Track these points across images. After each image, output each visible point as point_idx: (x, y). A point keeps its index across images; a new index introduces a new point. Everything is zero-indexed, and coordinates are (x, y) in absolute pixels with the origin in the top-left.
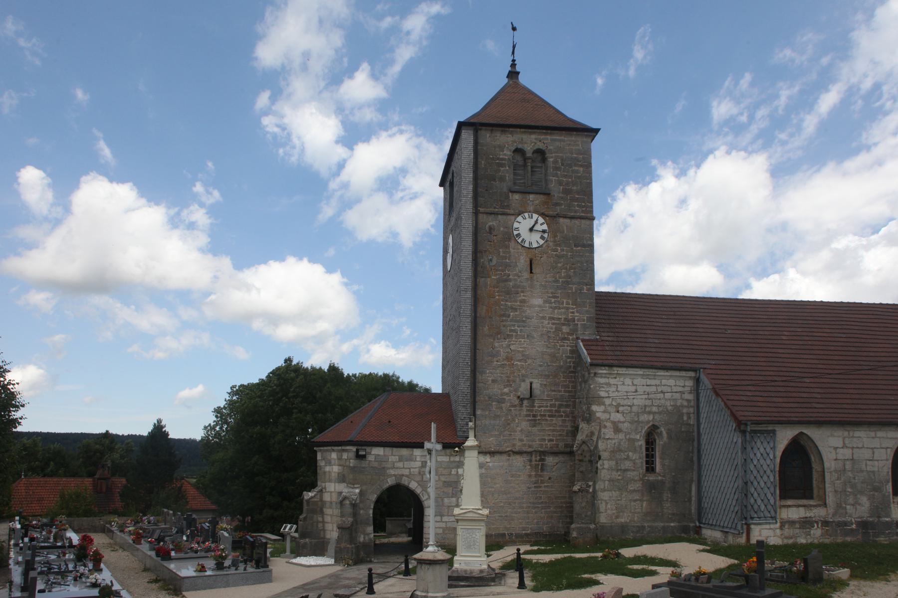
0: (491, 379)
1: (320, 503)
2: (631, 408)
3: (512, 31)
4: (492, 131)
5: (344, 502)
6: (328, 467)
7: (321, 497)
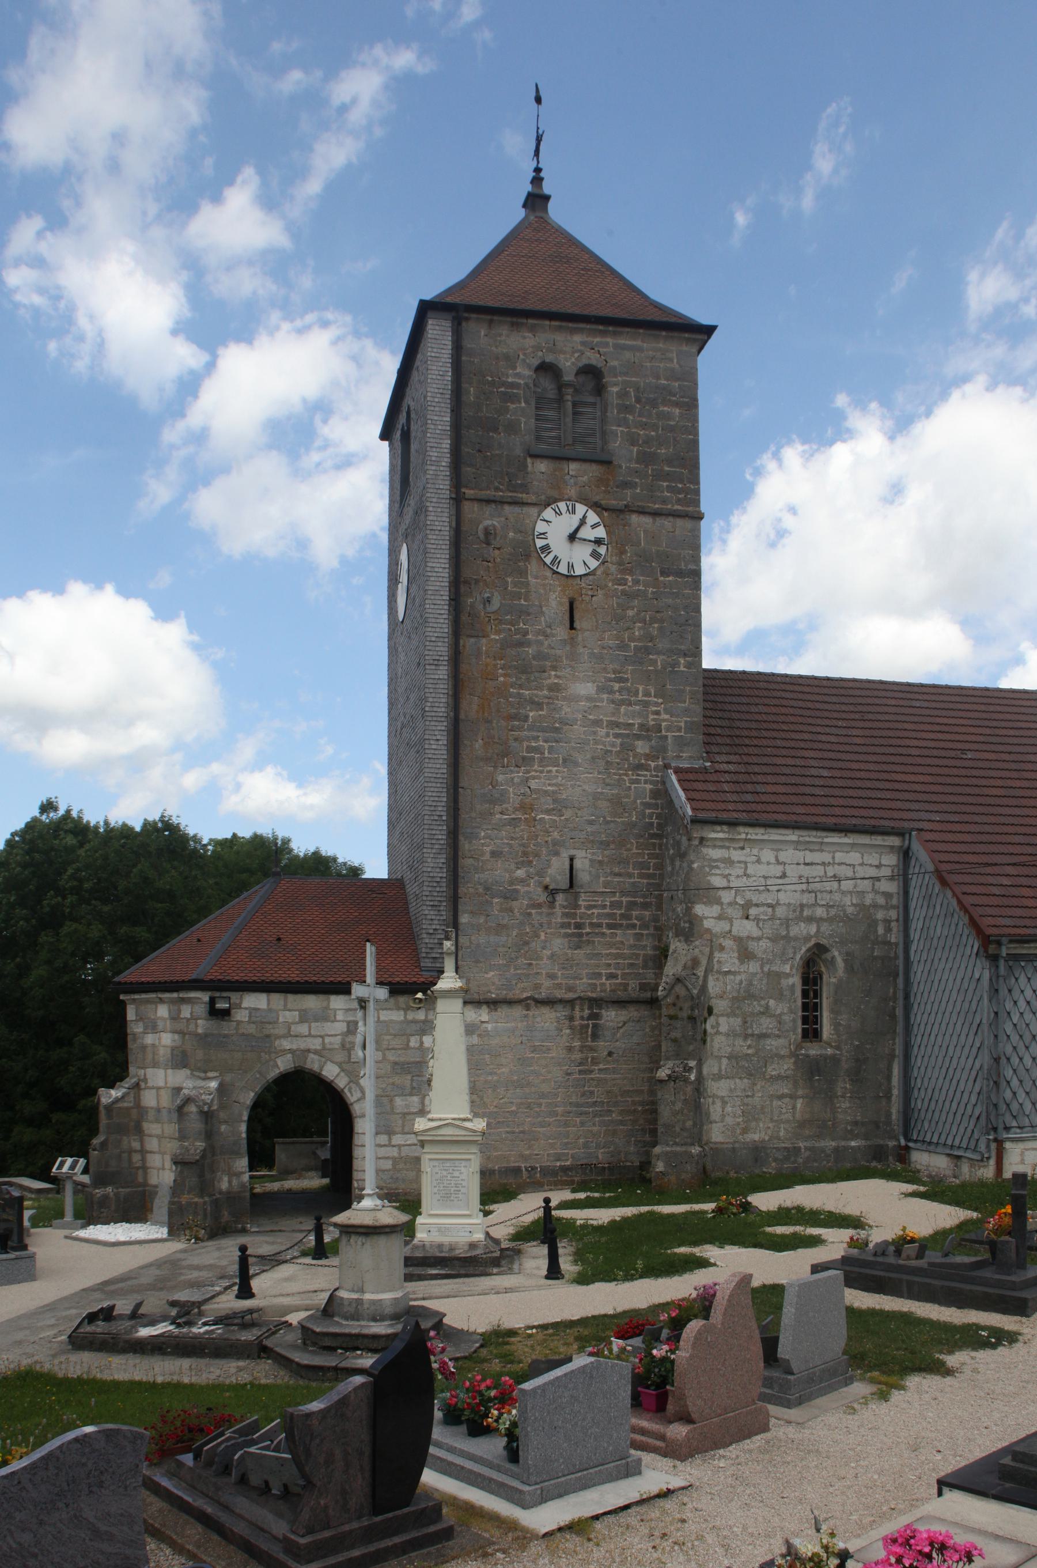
0: (488, 849)
1: (134, 1112)
3: (535, 105)
4: (491, 322)
5: (186, 1109)
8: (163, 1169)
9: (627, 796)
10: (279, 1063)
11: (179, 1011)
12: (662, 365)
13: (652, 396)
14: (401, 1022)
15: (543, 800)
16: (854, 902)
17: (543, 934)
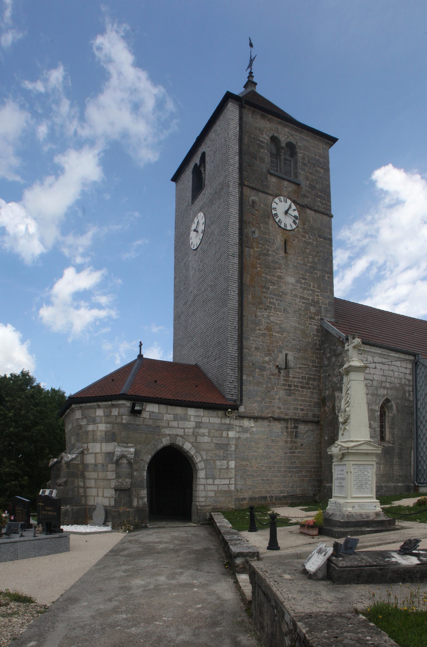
0: (254, 346)
1: (81, 466)
2: (372, 383)
3: (250, 47)
4: (254, 112)
5: (120, 462)
6: (91, 426)
7: (83, 459)
8: (98, 496)
10: (163, 441)
11: (111, 412)
12: (317, 151)
13: (313, 162)
14: (219, 424)
16: (399, 382)
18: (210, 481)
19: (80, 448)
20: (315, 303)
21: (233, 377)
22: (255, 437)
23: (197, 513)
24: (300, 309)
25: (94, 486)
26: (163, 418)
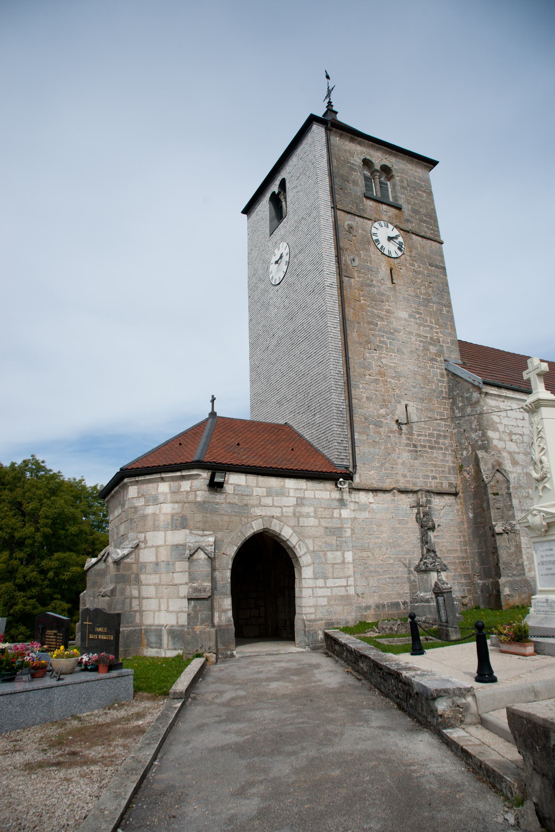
0: (365, 395)
1: (134, 567)
3: (327, 80)
5: (195, 556)
8: (159, 610)
9: (430, 375)
14: (328, 500)
15: (389, 371)
17: (397, 449)
18: (320, 582)
19: (135, 540)
20: (435, 342)
21: (342, 436)
22: (376, 517)
23: (305, 631)
24: (417, 349)
25: (154, 596)
26: (253, 493)
